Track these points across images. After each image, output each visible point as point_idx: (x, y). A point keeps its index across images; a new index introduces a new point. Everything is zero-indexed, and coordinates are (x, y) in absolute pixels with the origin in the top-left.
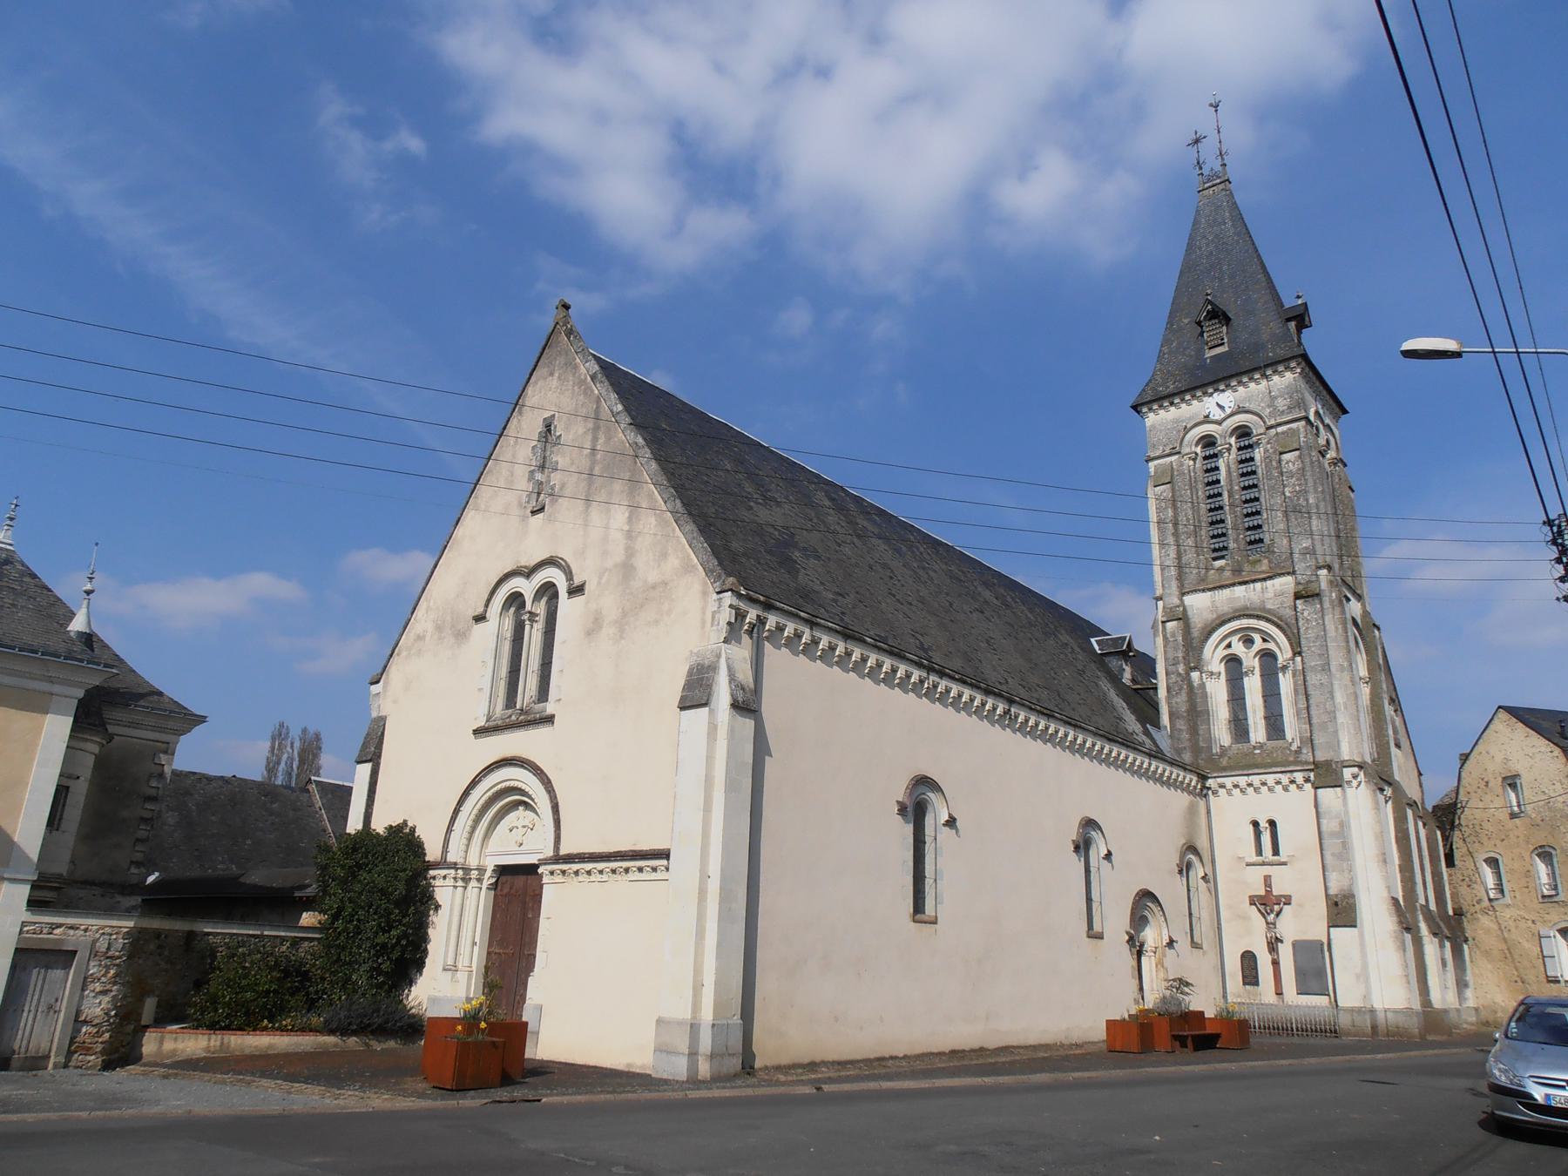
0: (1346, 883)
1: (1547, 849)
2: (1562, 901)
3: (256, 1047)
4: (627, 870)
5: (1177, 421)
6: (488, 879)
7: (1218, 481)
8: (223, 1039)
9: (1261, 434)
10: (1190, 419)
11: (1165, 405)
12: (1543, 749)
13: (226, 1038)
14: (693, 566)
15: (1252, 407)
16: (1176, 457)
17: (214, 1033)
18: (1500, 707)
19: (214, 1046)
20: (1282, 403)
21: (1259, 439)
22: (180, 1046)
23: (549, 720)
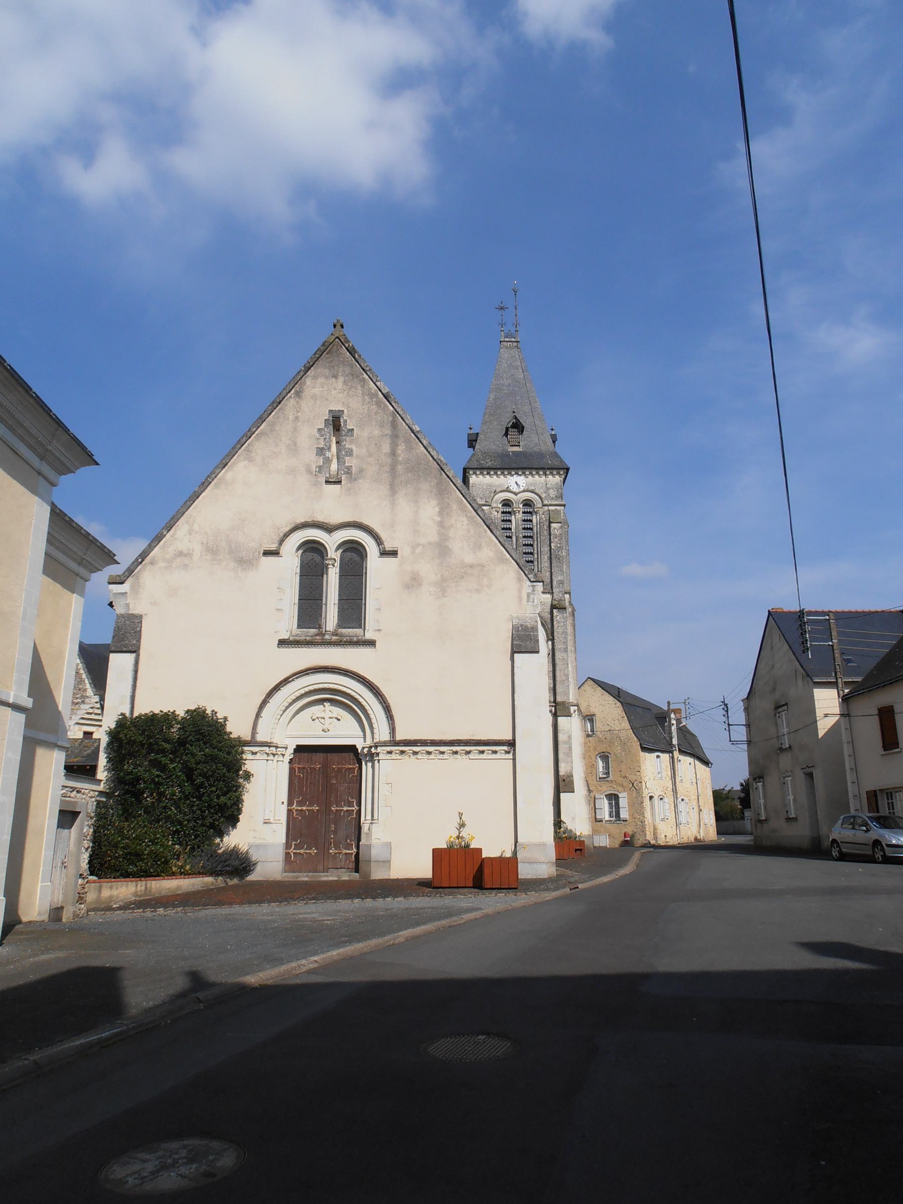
0: (569, 769)
1: (606, 754)
2: (611, 781)
3: (169, 888)
4: (468, 753)
5: (490, 485)
6: (289, 754)
7: (510, 529)
8: (146, 884)
9: (540, 508)
10: (498, 486)
11: (484, 473)
12: (610, 702)
13: (149, 882)
14: (507, 559)
15: (537, 491)
16: (488, 507)
17: (140, 880)
18: (589, 678)
19: (141, 891)
20: (552, 493)
21: (538, 510)
22: (115, 892)
23: (371, 643)
